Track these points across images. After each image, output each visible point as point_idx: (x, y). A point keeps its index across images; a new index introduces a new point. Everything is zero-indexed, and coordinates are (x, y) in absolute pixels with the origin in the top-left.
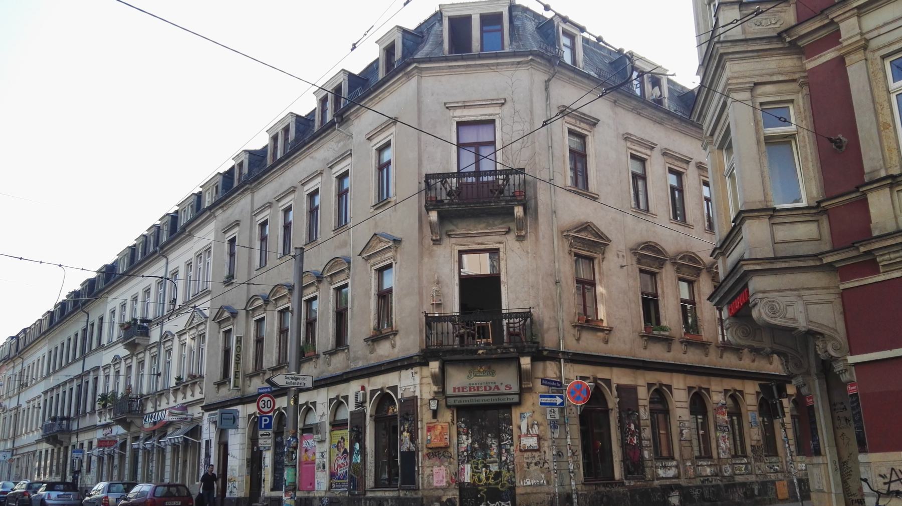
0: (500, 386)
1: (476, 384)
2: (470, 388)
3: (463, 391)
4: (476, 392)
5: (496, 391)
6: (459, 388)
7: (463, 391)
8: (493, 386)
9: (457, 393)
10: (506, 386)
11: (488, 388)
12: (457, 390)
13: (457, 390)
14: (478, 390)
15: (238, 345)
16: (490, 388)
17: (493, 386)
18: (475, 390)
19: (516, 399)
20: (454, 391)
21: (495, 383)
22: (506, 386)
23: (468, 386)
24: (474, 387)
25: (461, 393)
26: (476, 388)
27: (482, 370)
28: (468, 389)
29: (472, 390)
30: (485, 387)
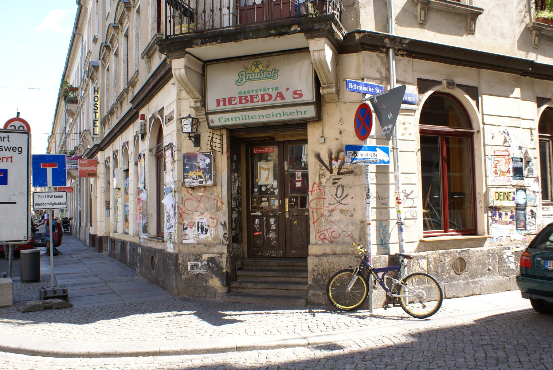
0: (284, 93)
1: (249, 92)
2: (240, 98)
3: (230, 104)
4: (249, 105)
5: (279, 101)
6: (224, 100)
7: (230, 104)
8: (274, 95)
9: (222, 107)
10: (295, 93)
11: (267, 97)
12: (221, 103)
13: (221, 103)
14: (252, 101)
15: (245, 349)
16: (270, 97)
17: (274, 95)
18: (247, 101)
19: (310, 112)
20: (218, 105)
21: (277, 89)
22: (295, 93)
23: (237, 95)
24: (246, 97)
25: (228, 107)
26: (249, 98)
27: (257, 71)
28: (237, 100)
29: (244, 101)
30: (263, 96)
